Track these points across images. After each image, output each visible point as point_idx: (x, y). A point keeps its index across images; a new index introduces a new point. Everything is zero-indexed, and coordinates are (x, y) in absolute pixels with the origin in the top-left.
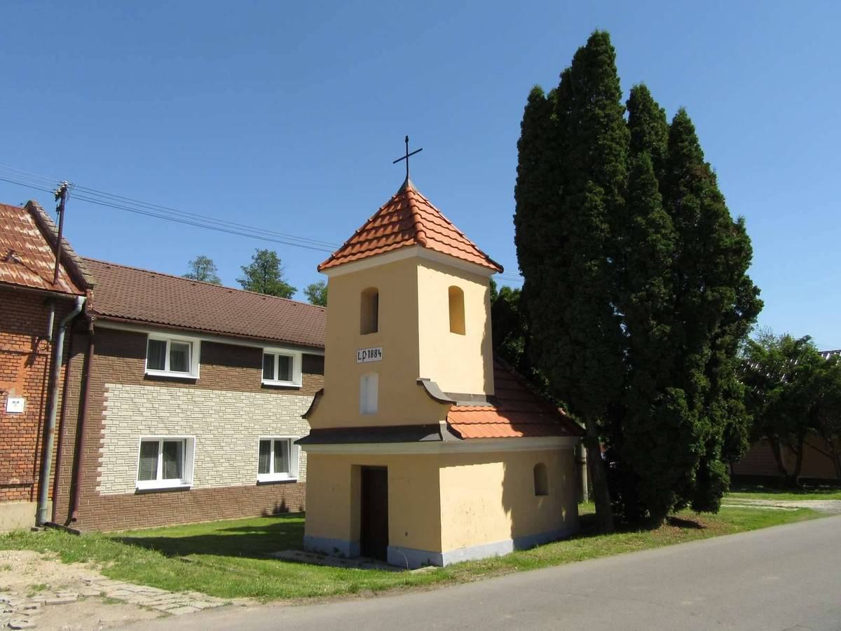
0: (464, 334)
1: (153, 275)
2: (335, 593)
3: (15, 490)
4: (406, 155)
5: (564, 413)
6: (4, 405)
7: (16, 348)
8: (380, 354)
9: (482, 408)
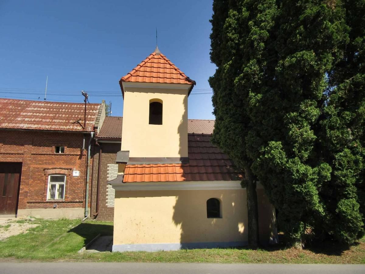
0: (149, 124)
1: (209, 121)
2: (10, 256)
3: (77, 203)
7: (75, 153)
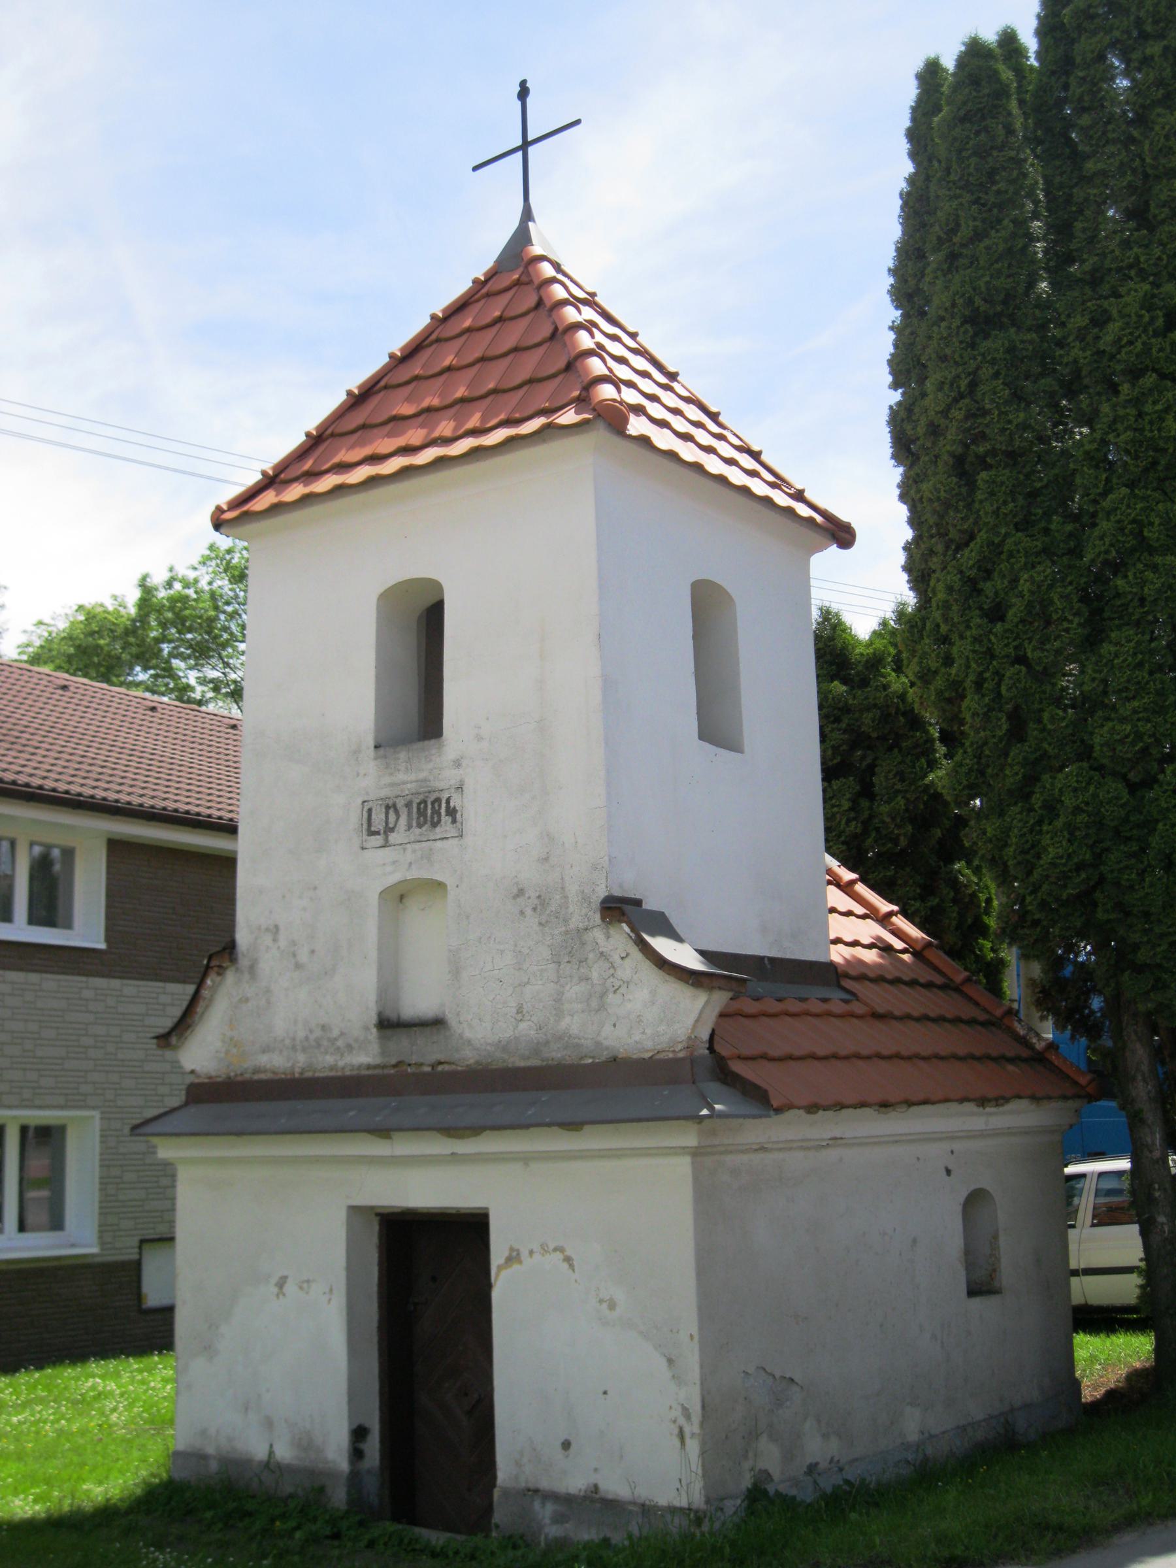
4: (519, 143)
6: (1158, 1350)
9: (825, 1006)
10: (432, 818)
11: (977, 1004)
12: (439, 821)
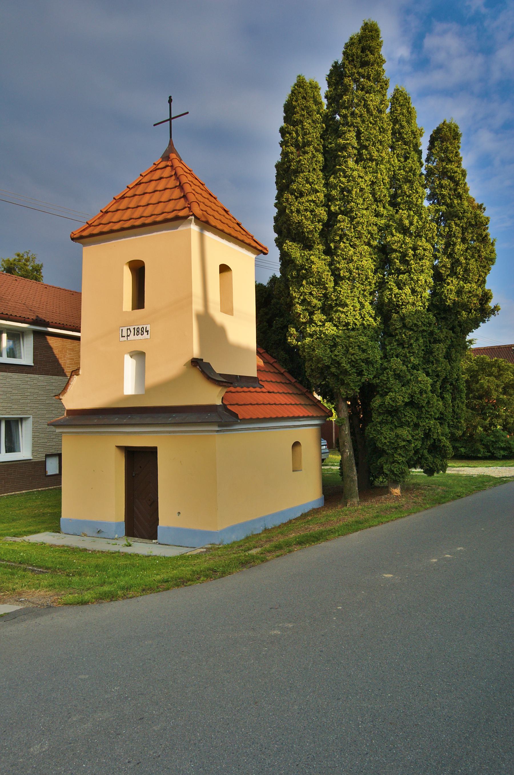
4: (172, 120)
5: (459, 549)
8: (147, 331)
10: (137, 333)
11: (276, 368)
12: (143, 334)
